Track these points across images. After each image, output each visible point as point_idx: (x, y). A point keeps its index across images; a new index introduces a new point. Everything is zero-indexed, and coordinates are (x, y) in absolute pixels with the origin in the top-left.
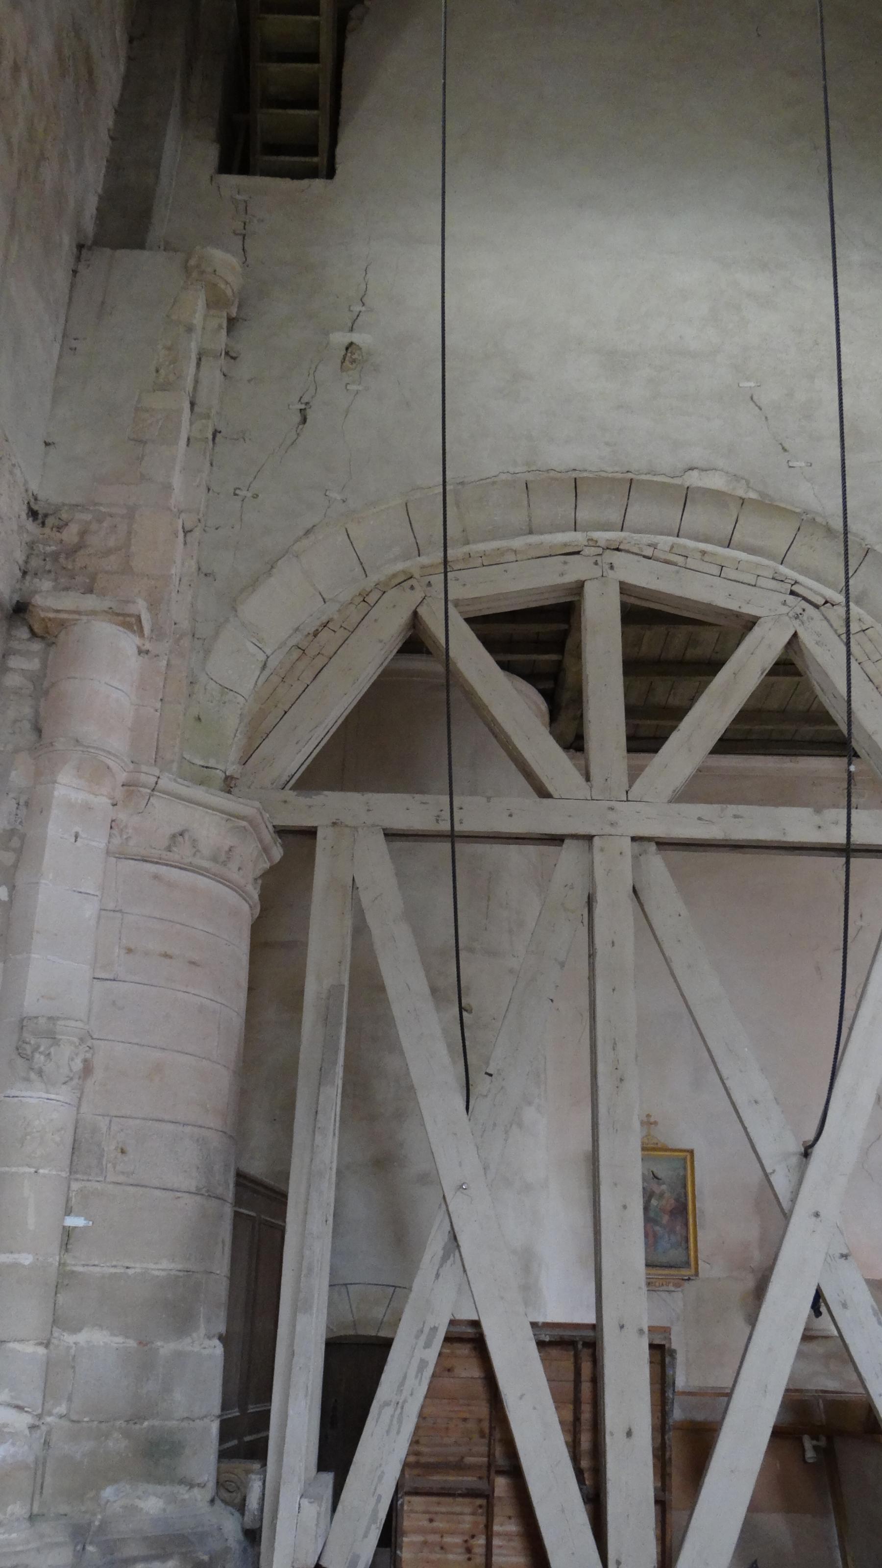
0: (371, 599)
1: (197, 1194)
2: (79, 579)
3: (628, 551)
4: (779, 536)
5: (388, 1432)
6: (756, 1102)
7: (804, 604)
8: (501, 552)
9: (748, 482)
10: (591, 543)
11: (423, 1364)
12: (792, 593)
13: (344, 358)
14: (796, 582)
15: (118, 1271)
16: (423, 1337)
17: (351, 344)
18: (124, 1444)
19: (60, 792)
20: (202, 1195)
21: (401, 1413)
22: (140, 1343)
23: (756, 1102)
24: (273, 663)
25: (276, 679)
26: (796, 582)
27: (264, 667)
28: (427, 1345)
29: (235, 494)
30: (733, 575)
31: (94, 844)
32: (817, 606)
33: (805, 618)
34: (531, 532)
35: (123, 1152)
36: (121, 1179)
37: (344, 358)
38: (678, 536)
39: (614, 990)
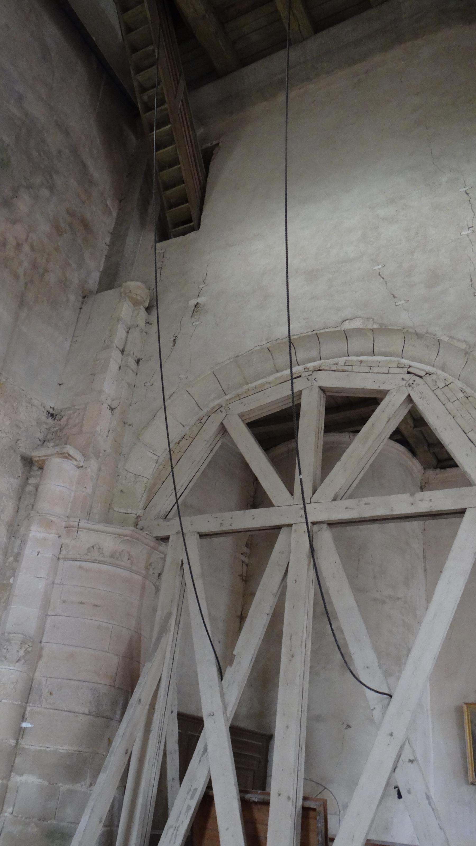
0: (203, 421)
1: (89, 715)
2: (63, 440)
3: (324, 370)
4: (396, 344)
5: (170, 842)
6: (368, 667)
7: (415, 378)
8: (263, 384)
9: (373, 320)
10: (306, 370)
11: (189, 807)
12: (409, 373)
13: (194, 311)
14: (410, 366)
15: (43, 749)
16: (191, 793)
17: (198, 303)
18: (36, 829)
19: (32, 534)
20: (93, 715)
21: (176, 833)
22: (49, 783)
23: (368, 667)
24: (161, 460)
25: (161, 467)
26: (410, 366)
27: (156, 463)
28: (192, 798)
29: (145, 386)
30: (376, 370)
31: (47, 555)
32: (421, 377)
33: (414, 385)
34: (277, 371)
35: (51, 693)
36: (48, 706)
37: (194, 311)
38: (321, 359)
39: (294, 607)
